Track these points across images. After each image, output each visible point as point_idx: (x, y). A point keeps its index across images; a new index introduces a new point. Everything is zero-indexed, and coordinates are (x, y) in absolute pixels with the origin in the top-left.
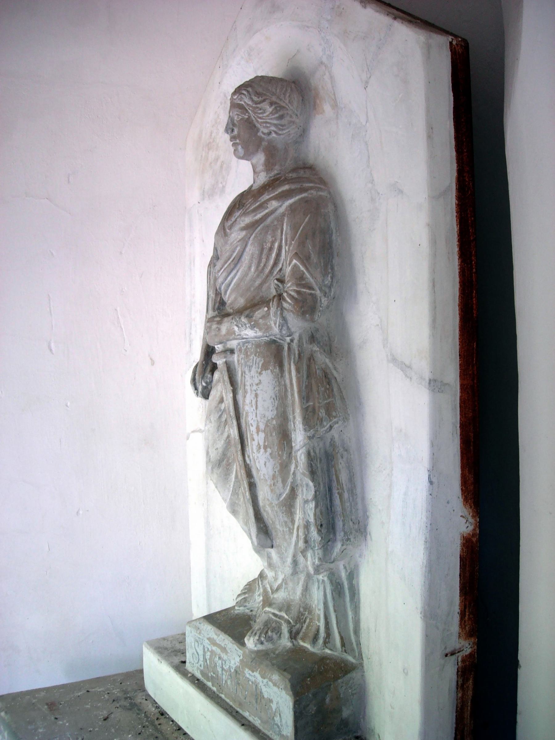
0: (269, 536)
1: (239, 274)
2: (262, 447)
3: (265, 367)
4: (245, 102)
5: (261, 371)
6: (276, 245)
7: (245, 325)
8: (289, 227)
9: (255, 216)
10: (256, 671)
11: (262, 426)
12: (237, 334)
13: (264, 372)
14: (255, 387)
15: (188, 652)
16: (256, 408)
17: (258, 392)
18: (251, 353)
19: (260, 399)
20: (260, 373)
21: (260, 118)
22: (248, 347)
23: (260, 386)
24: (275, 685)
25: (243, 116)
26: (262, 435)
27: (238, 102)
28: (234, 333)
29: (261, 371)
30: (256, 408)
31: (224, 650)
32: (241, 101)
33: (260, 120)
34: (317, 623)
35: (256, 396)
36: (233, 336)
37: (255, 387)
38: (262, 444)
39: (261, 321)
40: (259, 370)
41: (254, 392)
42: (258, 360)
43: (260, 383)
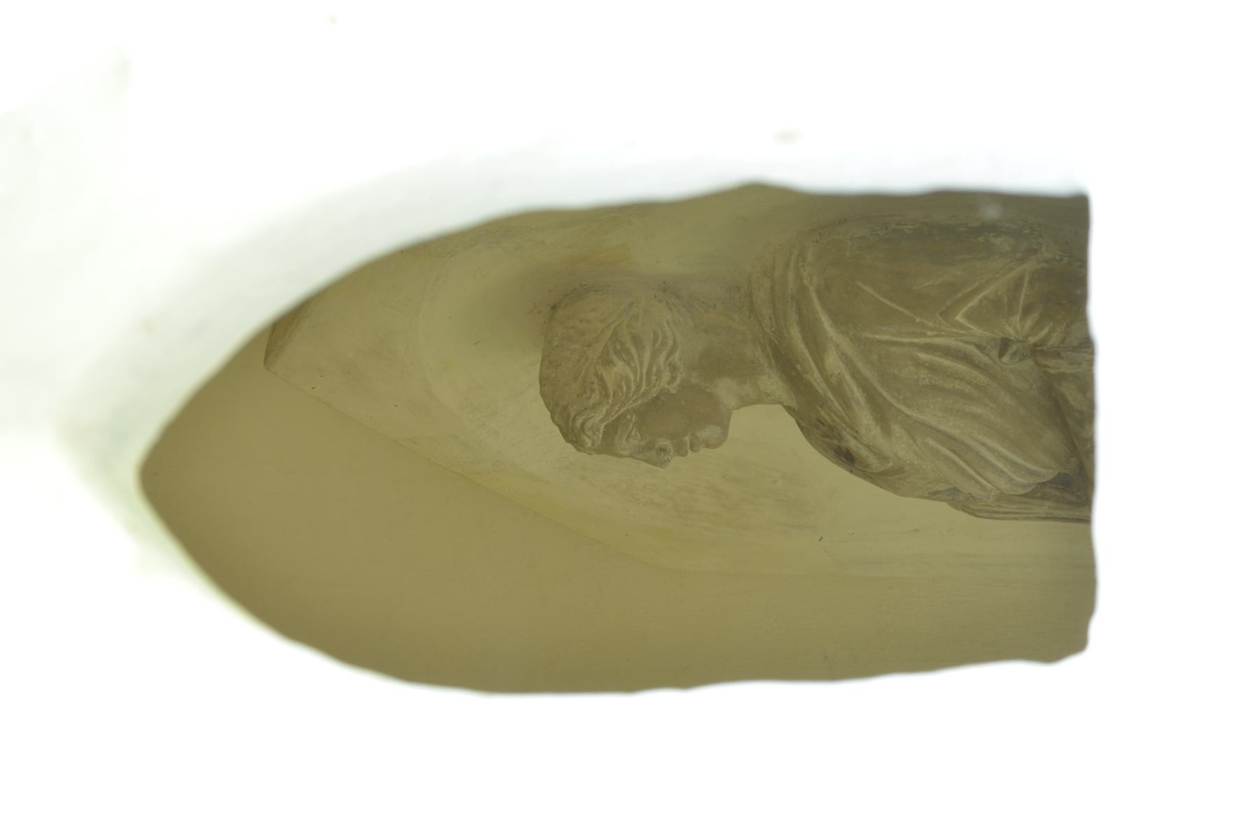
1: (989, 442)
4: (602, 421)
6: (923, 356)
21: (638, 387)
25: (631, 425)
27: (601, 436)
33: (644, 388)
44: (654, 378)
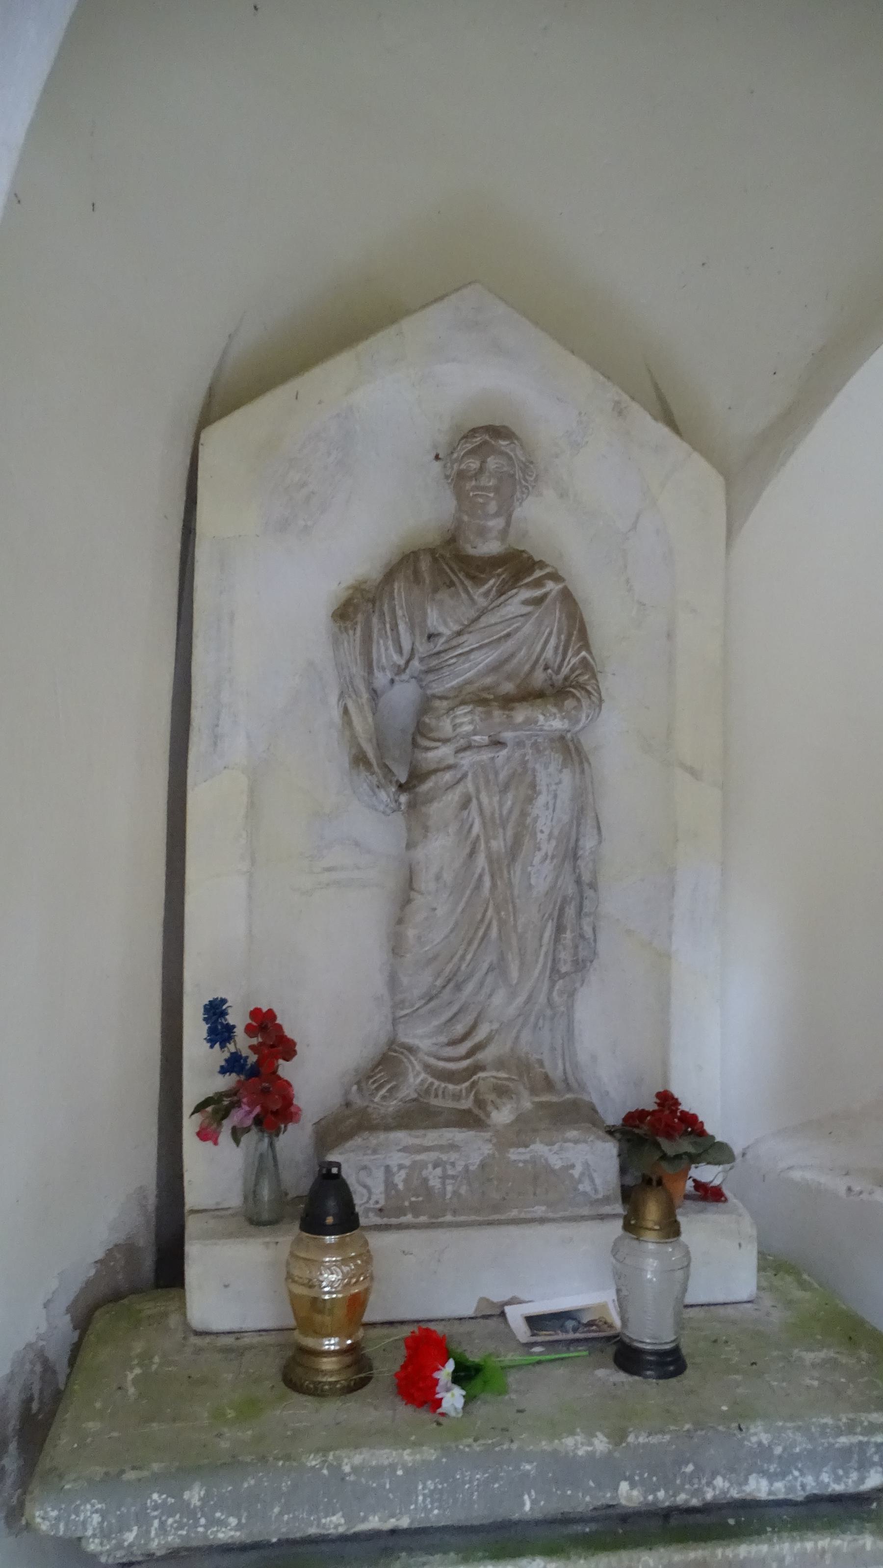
0: (245, 1116)
2: (549, 858)
3: (564, 765)
4: (516, 455)
5: (562, 769)
6: (548, 630)
7: (555, 714)
8: (564, 615)
9: (536, 592)
10: (534, 1142)
11: (556, 832)
12: (539, 723)
13: (564, 770)
14: (554, 787)
15: (307, 1237)
16: (554, 811)
17: (558, 792)
18: (545, 749)
19: (559, 801)
20: (561, 771)
21: (526, 481)
22: (539, 740)
23: (560, 786)
24: (576, 1142)
26: (554, 843)
28: (536, 722)
29: (562, 769)
30: (554, 811)
31: (453, 1147)
32: (512, 451)
33: (523, 482)
34: (541, 1070)
35: (555, 797)
36: (533, 725)
37: (554, 787)
38: (550, 854)
39: (573, 712)
40: (560, 767)
41: (553, 793)
42: (557, 755)
43: (560, 782)
44: (524, 489)
